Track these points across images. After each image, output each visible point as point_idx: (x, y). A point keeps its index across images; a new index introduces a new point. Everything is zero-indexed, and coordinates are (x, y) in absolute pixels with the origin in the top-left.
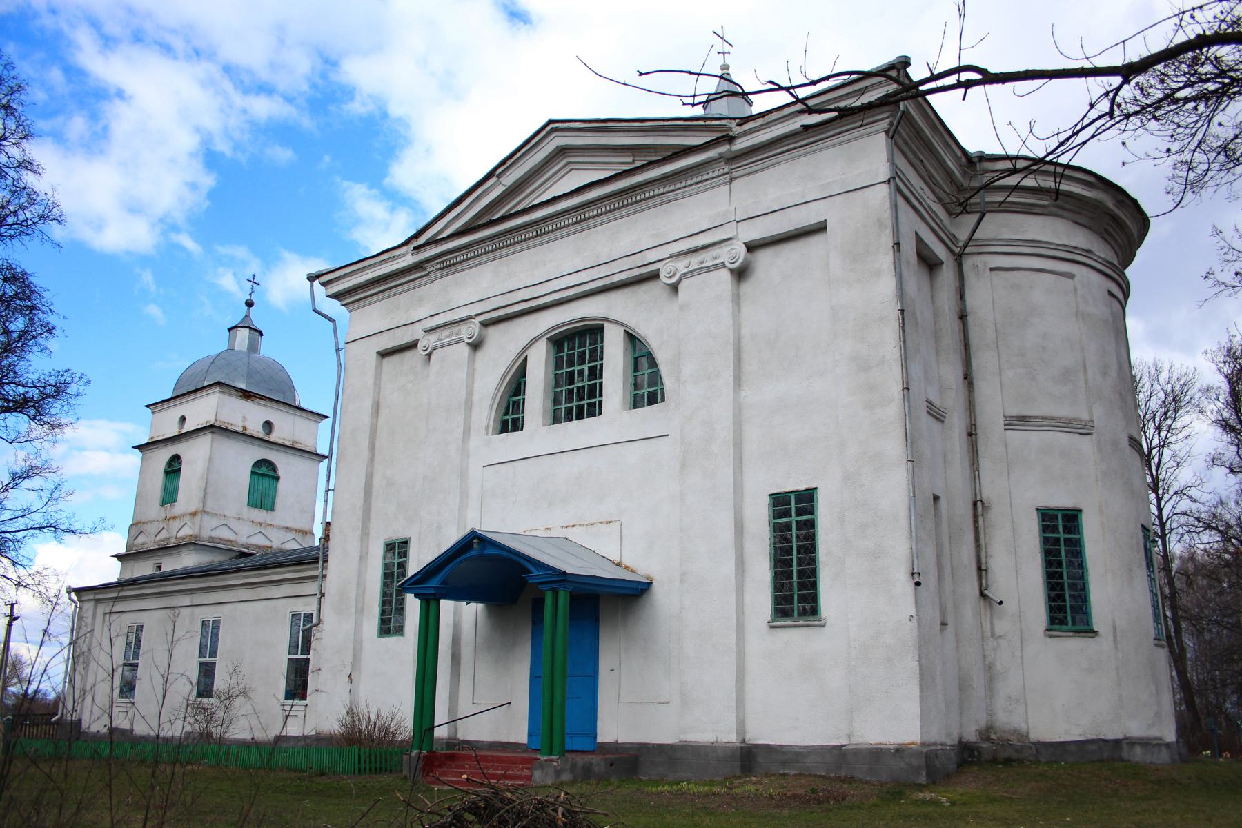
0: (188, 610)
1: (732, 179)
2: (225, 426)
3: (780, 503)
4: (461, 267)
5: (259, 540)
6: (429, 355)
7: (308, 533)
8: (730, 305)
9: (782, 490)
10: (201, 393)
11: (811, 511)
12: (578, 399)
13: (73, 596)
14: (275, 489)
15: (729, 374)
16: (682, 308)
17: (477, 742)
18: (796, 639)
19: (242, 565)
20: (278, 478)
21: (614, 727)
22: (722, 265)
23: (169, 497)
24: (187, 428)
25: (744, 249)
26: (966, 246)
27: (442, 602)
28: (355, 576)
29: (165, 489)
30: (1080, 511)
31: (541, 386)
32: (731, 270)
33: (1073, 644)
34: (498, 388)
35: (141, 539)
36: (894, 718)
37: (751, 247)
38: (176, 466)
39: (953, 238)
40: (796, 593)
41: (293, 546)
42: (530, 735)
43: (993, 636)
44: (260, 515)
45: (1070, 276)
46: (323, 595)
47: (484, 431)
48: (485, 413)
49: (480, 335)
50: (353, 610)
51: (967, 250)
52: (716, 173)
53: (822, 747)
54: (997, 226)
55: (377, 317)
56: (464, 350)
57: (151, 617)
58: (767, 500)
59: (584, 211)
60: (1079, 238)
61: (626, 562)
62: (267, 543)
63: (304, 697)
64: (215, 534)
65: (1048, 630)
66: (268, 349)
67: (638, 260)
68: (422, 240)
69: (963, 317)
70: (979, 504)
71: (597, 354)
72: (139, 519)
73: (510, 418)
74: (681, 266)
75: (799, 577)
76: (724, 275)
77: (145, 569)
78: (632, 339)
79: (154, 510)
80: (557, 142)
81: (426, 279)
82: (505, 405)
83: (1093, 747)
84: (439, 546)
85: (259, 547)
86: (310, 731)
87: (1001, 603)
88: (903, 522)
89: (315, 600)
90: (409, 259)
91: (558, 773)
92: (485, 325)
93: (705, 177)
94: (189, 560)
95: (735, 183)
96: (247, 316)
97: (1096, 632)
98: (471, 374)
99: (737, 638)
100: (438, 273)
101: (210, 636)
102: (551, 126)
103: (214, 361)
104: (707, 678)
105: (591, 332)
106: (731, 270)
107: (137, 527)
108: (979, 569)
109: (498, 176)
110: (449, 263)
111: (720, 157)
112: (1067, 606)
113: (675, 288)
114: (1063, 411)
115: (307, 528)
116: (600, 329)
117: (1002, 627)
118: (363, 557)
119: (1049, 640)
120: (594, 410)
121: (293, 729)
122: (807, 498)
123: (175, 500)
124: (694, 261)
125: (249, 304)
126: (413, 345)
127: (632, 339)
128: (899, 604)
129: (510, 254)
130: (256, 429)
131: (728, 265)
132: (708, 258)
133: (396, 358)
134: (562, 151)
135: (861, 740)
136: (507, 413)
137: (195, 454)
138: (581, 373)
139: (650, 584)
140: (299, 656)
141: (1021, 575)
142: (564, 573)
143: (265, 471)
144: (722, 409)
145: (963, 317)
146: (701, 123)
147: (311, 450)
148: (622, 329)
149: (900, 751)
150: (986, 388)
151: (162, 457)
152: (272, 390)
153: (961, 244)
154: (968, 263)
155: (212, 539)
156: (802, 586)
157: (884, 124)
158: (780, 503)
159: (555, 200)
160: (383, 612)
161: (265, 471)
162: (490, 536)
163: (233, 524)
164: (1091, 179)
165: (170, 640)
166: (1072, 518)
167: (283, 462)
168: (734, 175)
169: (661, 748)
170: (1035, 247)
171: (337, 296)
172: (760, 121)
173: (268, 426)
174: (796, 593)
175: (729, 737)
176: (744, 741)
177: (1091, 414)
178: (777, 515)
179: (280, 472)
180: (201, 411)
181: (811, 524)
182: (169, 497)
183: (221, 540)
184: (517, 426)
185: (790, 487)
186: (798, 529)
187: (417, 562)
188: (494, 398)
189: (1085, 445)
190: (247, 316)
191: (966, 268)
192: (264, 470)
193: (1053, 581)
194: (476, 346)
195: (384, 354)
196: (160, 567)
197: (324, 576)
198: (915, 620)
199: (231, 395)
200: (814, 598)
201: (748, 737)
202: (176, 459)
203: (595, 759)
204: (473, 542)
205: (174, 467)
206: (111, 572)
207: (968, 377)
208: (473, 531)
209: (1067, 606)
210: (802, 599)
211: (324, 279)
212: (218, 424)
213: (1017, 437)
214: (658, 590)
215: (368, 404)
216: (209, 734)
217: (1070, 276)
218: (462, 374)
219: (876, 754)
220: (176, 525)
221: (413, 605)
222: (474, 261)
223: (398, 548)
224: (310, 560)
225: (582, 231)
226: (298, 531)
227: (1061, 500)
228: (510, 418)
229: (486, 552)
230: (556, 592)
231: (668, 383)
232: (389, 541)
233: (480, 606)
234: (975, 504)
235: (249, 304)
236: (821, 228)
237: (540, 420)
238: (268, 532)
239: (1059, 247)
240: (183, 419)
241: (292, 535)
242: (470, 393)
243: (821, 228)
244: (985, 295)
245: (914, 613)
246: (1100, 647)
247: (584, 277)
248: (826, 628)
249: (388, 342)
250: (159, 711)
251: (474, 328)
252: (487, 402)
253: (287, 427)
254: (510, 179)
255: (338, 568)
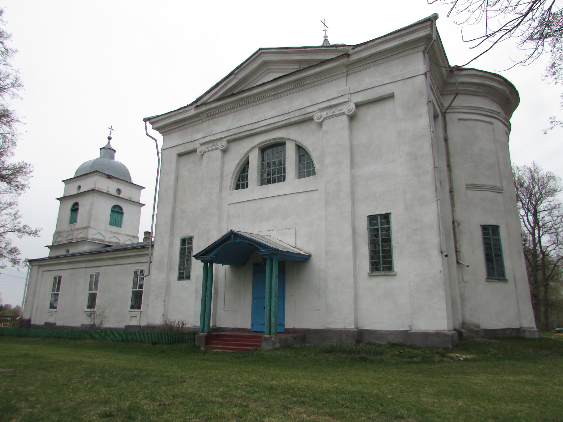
0: (83, 270)
1: (347, 75)
2: (100, 190)
3: (372, 219)
4: (217, 116)
5: (114, 240)
6: (202, 155)
7: (137, 237)
8: (348, 131)
9: (374, 214)
10: (89, 175)
11: (388, 223)
12: (273, 174)
13: (28, 263)
14: (122, 218)
15: (347, 162)
16: (324, 133)
17: (226, 328)
18: (381, 282)
19: (107, 252)
20: (123, 213)
21: (291, 323)
22: (344, 114)
23: (73, 220)
24: (81, 191)
25: (354, 106)
26: (448, 109)
27: (214, 264)
28: (167, 252)
29: (71, 217)
30: (498, 226)
31: (256, 169)
32: (348, 116)
33: (498, 285)
34: (235, 169)
35: (59, 239)
36: (435, 319)
37: (358, 106)
38: (76, 207)
39: (442, 104)
40: (381, 259)
41: (129, 242)
42: (252, 325)
43: (463, 281)
44: (115, 229)
45: (491, 123)
46: (151, 262)
47: (229, 188)
48: (229, 181)
49: (227, 146)
50: (166, 268)
51: (448, 111)
52: (340, 72)
53: (396, 331)
54: (461, 101)
55: (177, 139)
56: (219, 153)
57: (65, 274)
58: (366, 218)
59: (278, 90)
60: (495, 107)
61: (298, 246)
62: (118, 241)
63: (139, 308)
64: (94, 237)
65: (488, 279)
66: (118, 158)
67: (303, 112)
68: (199, 103)
69: (446, 140)
70: (456, 223)
71: (283, 154)
72: (60, 230)
73: (241, 182)
74: (324, 114)
75: (382, 253)
76: (345, 118)
77: (62, 252)
78: (299, 148)
79: (66, 226)
80: (263, 59)
81: (200, 121)
82: (238, 177)
83: (508, 332)
84: (208, 240)
85: (114, 242)
86: (143, 323)
87: (468, 266)
88: (436, 228)
89: (147, 264)
90: (193, 112)
91: (274, 344)
92: (229, 142)
93: (335, 74)
94: (86, 248)
95: (349, 77)
96: (109, 143)
97: (507, 280)
98: (223, 163)
99: (354, 281)
100: (206, 119)
101: (94, 283)
102: (260, 51)
103: (95, 162)
104: (343, 297)
105: (280, 144)
106: (348, 116)
107: (57, 234)
108: (456, 251)
109: (236, 74)
110: (212, 115)
111: (343, 64)
112: (495, 268)
113: (321, 124)
114: (491, 183)
115: (136, 235)
116: (283, 144)
117: (466, 278)
118: (171, 245)
119: (487, 283)
120: (282, 179)
121: (134, 323)
122: (386, 217)
123: (76, 222)
124: (330, 112)
125: (109, 138)
126: (194, 151)
127: (299, 148)
128: (435, 264)
129: (241, 110)
130: (114, 192)
131: (346, 113)
132: (337, 111)
133: (186, 157)
134: (265, 63)
135: (417, 328)
136: (239, 181)
137: (85, 204)
138: (274, 163)
139: (310, 256)
140: (138, 290)
141: (474, 254)
142: (278, 250)
143: (117, 211)
144: (345, 177)
145: (446, 140)
146: (334, 48)
147: (138, 201)
148: (294, 143)
149: (438, 334)
150: (456, 171)
151: (69, 204)
152: (120, 176)
153: (445, 108)
154: (448, 116)
155: (93, 239)
156: (384, 257)
157: (422, 48)
158: (372, 219)
159: (264, 84)
160: (180, 269)
161: (117, 211)
162: (240, 233)
163: (103, 233)
164: (502, 80)
165: (76, 285)
166: (495, 229)
167: (126, 208)
168: (349, 73)
169: (316, 331)
170: (477, 110)
171: (158, 129)
172: (363, 47)
173: (119, 191)
174: (381, 259)
175: (352, 327)
176: (357, 328)
177: (501, 184)
178: (371, 224)
179: (124, 211)
180: (86, 185)
181: (389, 229)
182: (73, 220)
183: (97, 240)
184: (245, 186)
185: (378, 213)
186: (382, 231)
187: (198, 247)
188: (233, 174)
189: (499, 197)
190: (109, 143)
191: (447, 118)
192: (117, 210)
193: (381, 269)
194: (224, 151)
195: (180, 155)
196: (68, 251)
197: (152, 254)
198: (442, 273)
199: (102, 177)
200: (390, 263)
201: (359, 326)
202: (76, 204)
203: (289, 336)
204: (232, 236)
205: (75, 209)
206: (45, 253)
207: (449, 166)
208: (232, 231)
209: (495, 268)
210: (384, 263)
211: (151, 121)
212: (96, 189)
213: (471, 193)
214: (315, 260)
215: (173, 177)
216: (94, 325)
217: (491, 123)
218: (219, 163)
219: (425, 335)
220: (76, 233)
221: (197, 267)
222: (224, 113)
223: (186, 242)
224: (145, 248)
225: (275, 99)
226: (131, 236)
227: (491, 222)
228: (241, 182)
229: (237, 241)
230: (272, 260)
231: (317, 167)
232: (183, 238)
233: (228, 266)
234: (453, 222)
235: (109, 138)
236: (391, 96)
237: (255, 183)
238: (118, 236)
239: (487, 110)
240: (79, 187)
241: (129, 238)
242: (222, 172)
243: (391, 96)
244: (456, 131)
245: (442, 270)
246: (509, 286)
247: (277, 119)
248: (396, 277)
249: (182, 150)
250: (72, 313)
251: (224, 143)
252: (230, 176)
253: (126, 192)
254: (241, 76)
255: (158, 251)
